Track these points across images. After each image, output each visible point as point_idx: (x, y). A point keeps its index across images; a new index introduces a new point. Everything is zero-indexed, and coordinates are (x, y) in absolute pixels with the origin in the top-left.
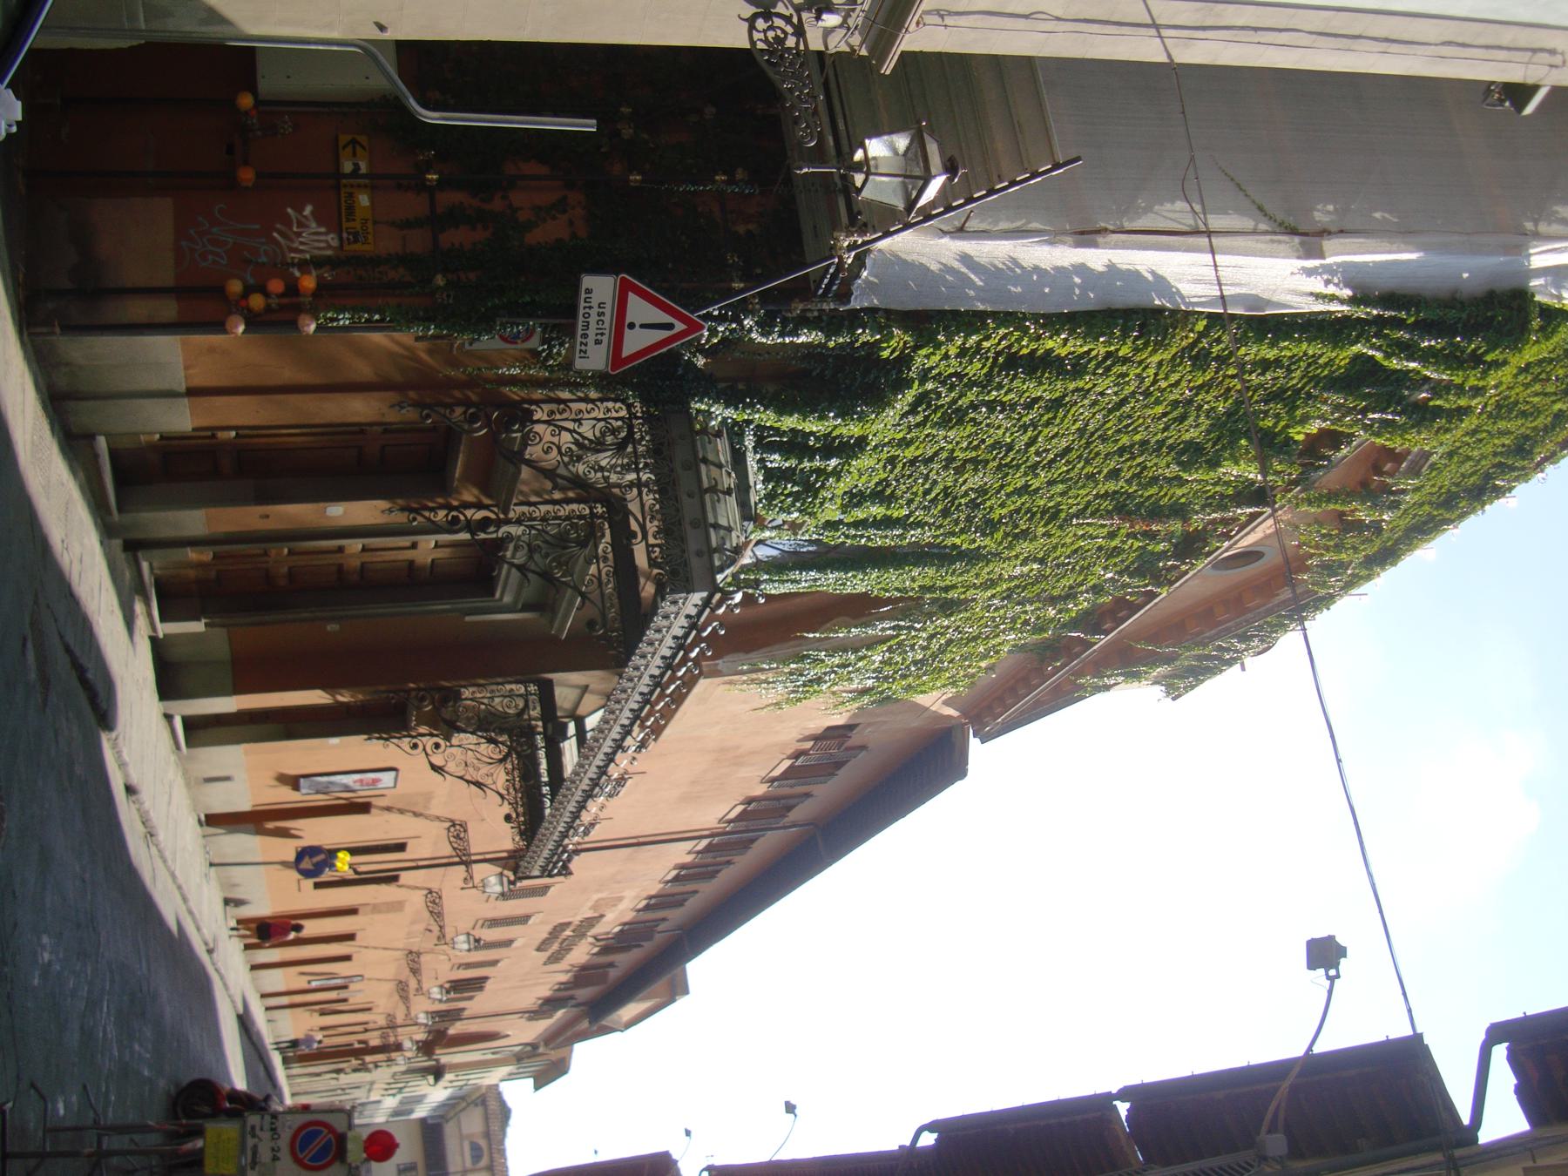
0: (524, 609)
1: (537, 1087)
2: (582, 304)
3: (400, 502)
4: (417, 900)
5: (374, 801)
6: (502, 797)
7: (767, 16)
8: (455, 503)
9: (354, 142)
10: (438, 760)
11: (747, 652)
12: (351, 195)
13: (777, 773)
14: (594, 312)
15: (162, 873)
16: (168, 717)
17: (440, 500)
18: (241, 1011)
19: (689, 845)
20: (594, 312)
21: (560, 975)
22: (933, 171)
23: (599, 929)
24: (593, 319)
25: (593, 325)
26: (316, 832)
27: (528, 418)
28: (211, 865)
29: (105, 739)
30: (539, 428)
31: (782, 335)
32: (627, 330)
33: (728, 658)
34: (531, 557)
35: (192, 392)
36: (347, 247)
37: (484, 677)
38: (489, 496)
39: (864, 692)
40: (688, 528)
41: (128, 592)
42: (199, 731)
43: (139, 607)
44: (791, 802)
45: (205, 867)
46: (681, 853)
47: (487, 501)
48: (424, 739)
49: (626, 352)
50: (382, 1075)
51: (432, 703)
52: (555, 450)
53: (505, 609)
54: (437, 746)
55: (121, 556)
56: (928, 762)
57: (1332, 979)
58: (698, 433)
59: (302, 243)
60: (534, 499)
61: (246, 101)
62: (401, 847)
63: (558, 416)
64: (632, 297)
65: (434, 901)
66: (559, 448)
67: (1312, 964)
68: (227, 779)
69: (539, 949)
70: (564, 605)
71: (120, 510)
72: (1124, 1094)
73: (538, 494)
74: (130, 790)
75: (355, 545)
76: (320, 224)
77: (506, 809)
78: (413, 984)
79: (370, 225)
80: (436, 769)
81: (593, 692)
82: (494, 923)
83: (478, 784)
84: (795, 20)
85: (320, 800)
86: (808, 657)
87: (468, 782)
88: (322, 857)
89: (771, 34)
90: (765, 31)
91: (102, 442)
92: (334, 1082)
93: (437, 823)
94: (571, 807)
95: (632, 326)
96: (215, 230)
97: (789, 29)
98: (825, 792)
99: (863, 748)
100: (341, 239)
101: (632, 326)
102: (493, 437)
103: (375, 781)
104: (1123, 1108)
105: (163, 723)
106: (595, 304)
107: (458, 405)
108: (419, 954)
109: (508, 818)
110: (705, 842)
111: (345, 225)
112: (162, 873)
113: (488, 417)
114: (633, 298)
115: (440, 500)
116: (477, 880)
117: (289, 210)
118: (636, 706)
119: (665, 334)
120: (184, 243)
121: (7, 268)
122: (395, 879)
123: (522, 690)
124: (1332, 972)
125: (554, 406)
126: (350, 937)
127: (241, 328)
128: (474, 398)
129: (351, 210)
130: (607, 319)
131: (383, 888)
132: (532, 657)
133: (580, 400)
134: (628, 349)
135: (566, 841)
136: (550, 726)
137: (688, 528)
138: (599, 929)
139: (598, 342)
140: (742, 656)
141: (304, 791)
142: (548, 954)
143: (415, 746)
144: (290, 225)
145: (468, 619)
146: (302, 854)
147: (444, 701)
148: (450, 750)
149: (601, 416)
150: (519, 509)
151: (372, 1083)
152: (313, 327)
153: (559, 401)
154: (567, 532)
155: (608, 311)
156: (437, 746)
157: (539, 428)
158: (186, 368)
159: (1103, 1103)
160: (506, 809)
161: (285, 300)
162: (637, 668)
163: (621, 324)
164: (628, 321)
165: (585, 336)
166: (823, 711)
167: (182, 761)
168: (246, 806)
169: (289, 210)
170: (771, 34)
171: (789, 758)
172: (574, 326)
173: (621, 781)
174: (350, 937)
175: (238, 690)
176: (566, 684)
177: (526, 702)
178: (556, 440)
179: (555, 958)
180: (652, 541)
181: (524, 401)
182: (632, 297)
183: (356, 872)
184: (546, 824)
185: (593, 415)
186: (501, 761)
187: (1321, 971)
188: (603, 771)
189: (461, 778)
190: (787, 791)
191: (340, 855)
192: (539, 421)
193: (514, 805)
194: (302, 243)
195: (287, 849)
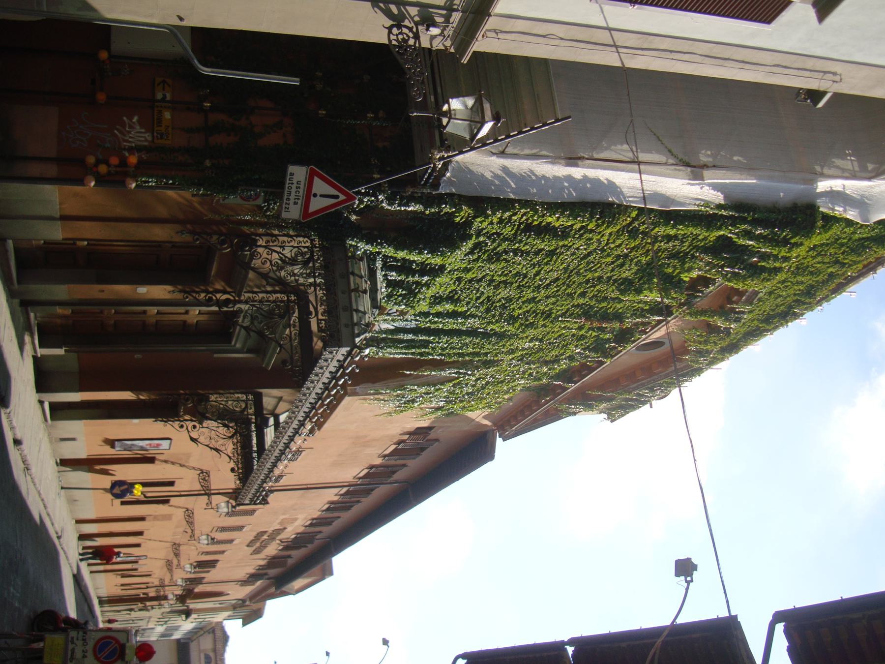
0: (248, 352)
1: (244, 624)
2: (288, 182)
3: (180, 287)
4: (179, 514)
5: (157, 456)
7: (399, 26)
8: (211, 290)
9: (164, 82)
10: (194, 435)
13: (387, 452)
14: (294, 186)
16: (41, 403)
18: (75, 572)
19: (336, 490)
20: (294, 186)
21: (260, 560)
22: (487, 119)
23: (282, 536)
24: (294, 190)
25: (293, 194)
26: (123, 472)
27: (254, 244)
28: (62, 488)
30: (260, 250)
31: (400, 205)
34: (252, 323)
36: (156, 141)
38: (231, 287)
39: (439, 409)
43: (27, 338)
44: (395, 469)
47: (229, 289)
50: (156, 613)
52: (269, 263)
53: (237, 351)
54: (194, 427)
55: (18, 309)
56: (470, 452)
57: (688, 583)
60: (256, 290)
61: (104, 55)
63: (271, 244)
65: (189, 515)
66: (271, 262)
67: (678, 574)
68: (74, 439)
69: (248, 546)
70: (270, 351)
71: (19, 282)
72: (572, 642)
75: (154, 310)
77: (232, 465)
78: (175, 562)
80: (192, 439)
81: (285, 401)
82: (223, 529)
83: (217, 450)
84: (414, 30)
85: (127, 454)
87: (211, 448)
88: (126, 487)
89: (400, 37)
90: (397, 35)
92: (128, 616)
93: (193, 471)
94: (269, 465)
95: (315, 195)
97: (411, 35)
99: (437, 440)
100: (153, 136)
101: (315, 195)
103: (158, 445)
104: (570, 650)
105: (38, 405)
106: (295, 182)
108: (179, 545)
109: (233, 470)
110: (345, 489)
111: (156, 129)
113: (232, 242)
114: (317, 181)
115: (202, 288)
116: (214, 504)
117: (125, 118)
118: (307, 410)
119: (334, 201)
122: (167, 501)
124: (689, 579)
125: (269, 238)
126: (140, 533)
127: (93, 184)
130: (301, 190)
131: (161, 506)
133: (284, 235)
138: (282, 536)
139: (295, 203)
140: (370, 385)
141: (118, 449)
142: (254, 548)
143: (182, 426)
145: (215, 355)
146: (115, 484)
148: (201, 430)
149: (296, 245)
151: (150, 618)
152: (134, 185)
153: (273, 235)
154: (274, 310)
155: (302, 186)
156: (194, 427)
157: (260, 250)
158: (60, 204)
159: (557, 648)
160: (232, 465)
162: (308, 389)
163: (309, 194)
164: (314, 191)
165: (288, 199)
166: (415, 419)
169: (125, 118)
170: (400, 37)
172: (283, 193)
173: (299, 452)
174: (140, 533)
176: (270, 397)
178: (269, 257)
179: (257, 551)
183: (145, 497)
185: (291, 244)
187: (683, 578)
188: (287, 446)
190: (392, 462)
192: (260, 246)
193: (237, 463)
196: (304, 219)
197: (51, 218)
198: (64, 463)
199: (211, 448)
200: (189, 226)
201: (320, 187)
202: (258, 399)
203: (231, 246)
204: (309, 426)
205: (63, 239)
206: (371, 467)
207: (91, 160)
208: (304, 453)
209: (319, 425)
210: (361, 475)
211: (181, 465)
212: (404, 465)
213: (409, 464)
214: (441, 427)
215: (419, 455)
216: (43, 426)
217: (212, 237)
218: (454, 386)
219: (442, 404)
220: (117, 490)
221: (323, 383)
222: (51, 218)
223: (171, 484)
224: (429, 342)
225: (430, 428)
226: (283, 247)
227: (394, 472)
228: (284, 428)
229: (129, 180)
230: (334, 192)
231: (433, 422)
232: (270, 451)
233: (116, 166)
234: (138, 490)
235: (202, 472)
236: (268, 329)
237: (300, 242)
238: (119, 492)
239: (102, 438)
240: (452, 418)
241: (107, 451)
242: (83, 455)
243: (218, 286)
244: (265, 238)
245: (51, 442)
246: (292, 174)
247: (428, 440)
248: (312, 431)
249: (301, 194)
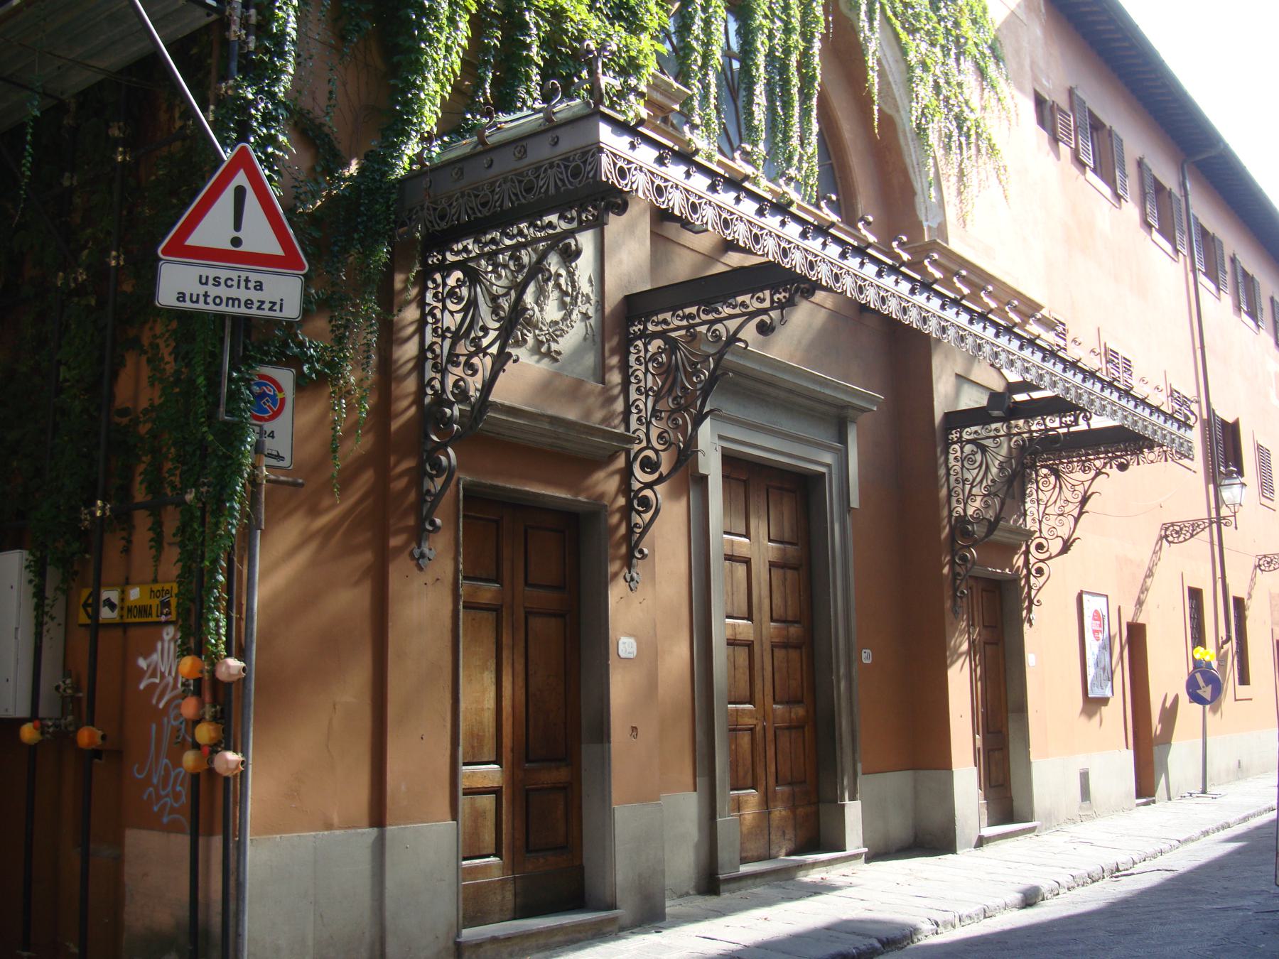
0: (843, 439)
2: (201, 306)
3: (614, 567)
4: (1266, 580)
5: (1127, 617)
6: (1097, 475)
8: (1025, 572)
10: (1056, 546)
11: (914, 193)
12: (130, 610)
13: (1107, 191)
14: (213, 291)
15: (1161, 862)
16: (981, 842)
17: (615, 519)
19: (1207, 299)
20: (213, 291)
24: (223, 292)
25: (233, 293)
26: (1167, 677)
27: (963, 519)
28: (1204, 792)
29: (928, 939)
30: (970, 511)
31: (282, 55)
32: (244, 248)
33: (922, 216)
35: (378, 817)
36: (173, 617)
37: (937, 489)
38: (1021, 546)
39: (982, 73)
40: (526, 161)
41: (785, 884)
42: (1007, 801)
43: (814, 876)
44: (1148, 181)
45: (1205, 799)
46: (1219, 307)
47: (1024, 548)
48: (1032, 560)
49: (277, 250)
51: (968, 547)
53: (849, 466)
54: (1040, 547)
55: (725, 898)
58: (423, 165)
59: (170, 673)
60: (619, 406)
61: (28, 733)
62: (1195, 595)
64: (193, 240)
68: (1085, 777)
70: (828, 392)
71: (612, 906)
73: (612, 400)
74: (1030, 899)
75: (722, 628)
76: (154, 650)
77: (1114, 472)
79: (157, 587)
80: (1066, 548)
81: (969, 369)
83: (1084, 500)
85: (1122, 676)
86: (919, 126)
87: (1081, 513)
88: (1198, 676)
91: (468, 934)
93: (1163, 554)
94: (1158, 420)
95: (236, 242)
96: (155, 781)
98: (1135, 143)
99: (1071, 92)
100: (167, 623)
101: (236, 242)
102: (455, 440)
103: (1097, 616)
105: (988, 849)
106: (201, 290)
107: (420, 484)
110: (1202, 279)
111: (154, 619)
112: (1161, 862)
113: (963, 547)
114: (196, 239)
115: (1023, 582)
117: (142, 687)
118: (1176, 425)
119: (251, 199)
120: (165, 820)
121: (548, 953)
123: (957, 447)
125: (954, 500)
127: (231, 756)
128: (408, 464)
129: (144, 610)
130: (223, 274)
131: (1250, 614)
132: (915, 442)
133: (948, 480)
134: (273, 247)
135: (632, 97)
136: (996, 413)
137: (526, 161)
139: (259, 286)
140: (919, 200)
141: (1108, 693)
143: (1040, 571)
144: (154, 686)
145: (855, 503)
146: (1196, 698)
147: (967, 534)
148: (1045, 534)
149: (642, 368)
150: (634, 425)
152: (234, 663)
153: (949, 496)
154: (661, 364)
155: (212, 273)
156: (1040, 547)
157: (970, 511)
158: (329, 826)
161: (207, 697)
162: (1155, 432)
163: (234, 256)
164: (228, 246)
165: (248, 303)
166: (1009, 119)
167: (1053, 822)
168: (1129, 756)
169: (142, 687)
171: (1084, 173)
172: (236, 319)
173: (1111, 356)
175: (943, 762)
176: (946, 394)
177: (968, 442)
180: (767, 304)
181: (950, 521)
182: (193, 240)
184: (1127, 424)
185: (641, 376)
186: (1058, 477)
188: (1169, 417)
189: (1077, 520)
190: (1229, 278)
191: (1197, 657)
192: (965, 510)
194: (170, 673)
195: (1189, 712)
196: (301, 267)
197: (379, 848)
198: (1145, 788)
199: (1081, 513)
200: (395, 542)
201: (213, 229)
202: (958, 419)
203: (442, 447)
204: (1034, 328)
205: (454, 817)
206: (1238, 308)
207: (189, 758)
208: (1110, 346)
209: (1030, 309)
210: (1168, 247)
211: (1150, 574)
212: (1233, 260)
213: (1138, 154)
214: (1035, 79)
215: (1110, 132)
216: (1045, 837)
217: (636, 525)
218: (912, 31)
219: (967, 65)
220: (1206, 692)
221: (1179, 429)
222: (379, 848)
223: (1195, 595)
224: (770, 55)
225: (1040, 102)
226: (965, 480)
227: (1159, 188)
228: (1125, 417)
229: (222, 674)
230: (227, 197)
231: (1021, 89)
232: (1027, 370)
233: (201, 704)
234: (1207, 654)
235: (1166, 536)
236: (697, 373)
237: (638, 359)
238: (1209, 688)
239: (1083, 719)
240: (1007, 51)
241: (1116, 713)
242: (1126, 759)
243: (1021, 562)
244: (954, 504)
245: (1089, 818)
246: (181, 297)
247: (1072, 109)
248: (1049, 324)
249: (234, 275)
